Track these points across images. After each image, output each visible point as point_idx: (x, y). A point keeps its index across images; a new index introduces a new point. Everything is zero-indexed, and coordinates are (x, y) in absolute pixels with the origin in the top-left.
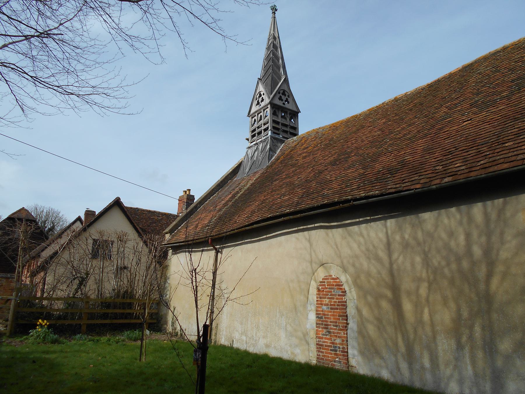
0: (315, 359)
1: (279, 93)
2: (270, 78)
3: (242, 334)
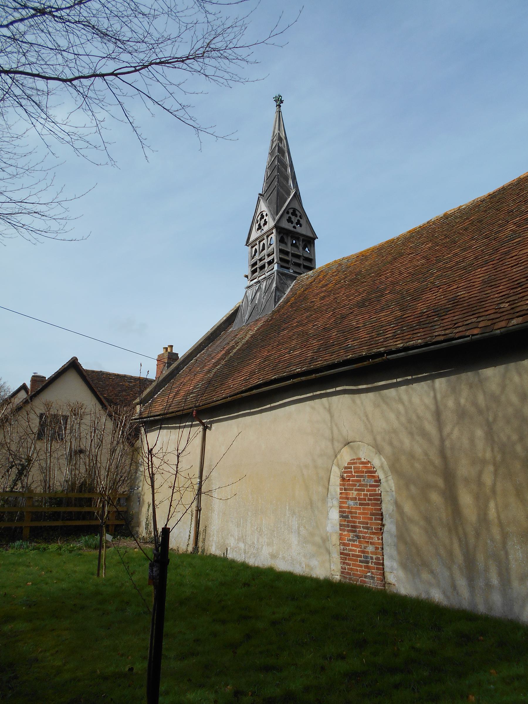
0: (339, 574)
1: (288, 213)
2: (275, 193)
3: (238, 540)
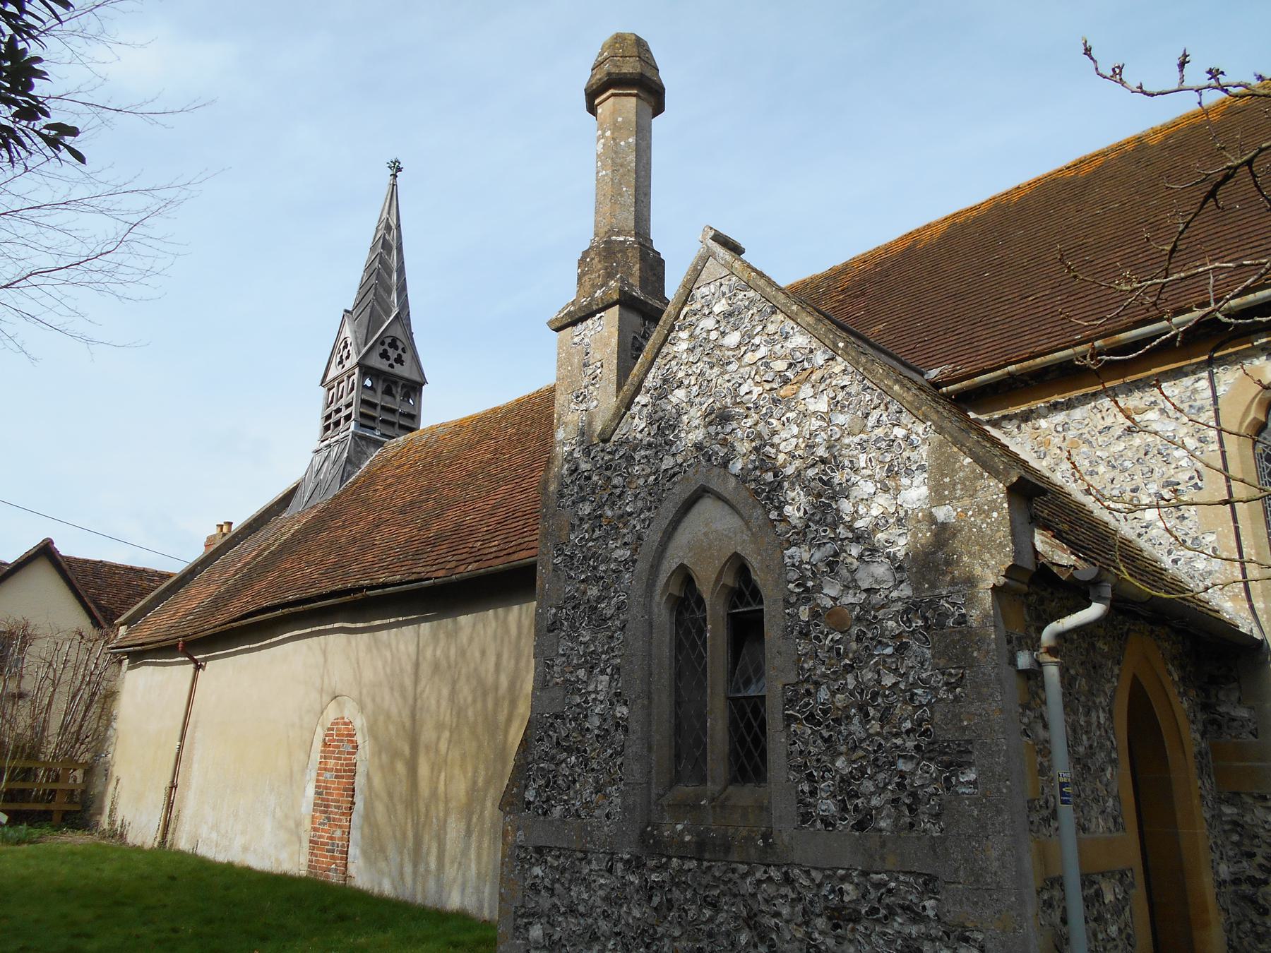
1: (383, 343)
2: (368, 310)
